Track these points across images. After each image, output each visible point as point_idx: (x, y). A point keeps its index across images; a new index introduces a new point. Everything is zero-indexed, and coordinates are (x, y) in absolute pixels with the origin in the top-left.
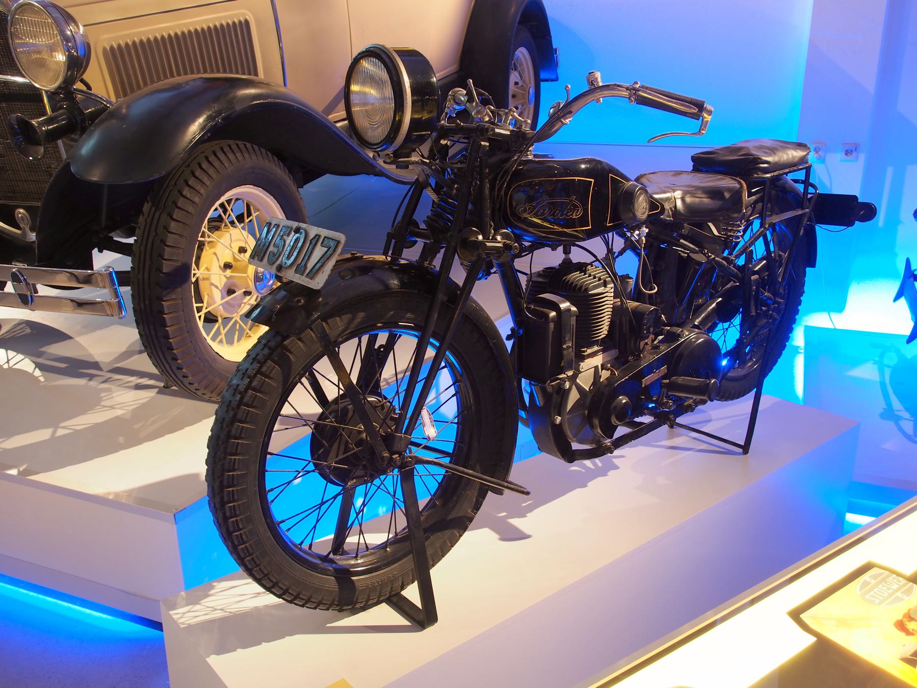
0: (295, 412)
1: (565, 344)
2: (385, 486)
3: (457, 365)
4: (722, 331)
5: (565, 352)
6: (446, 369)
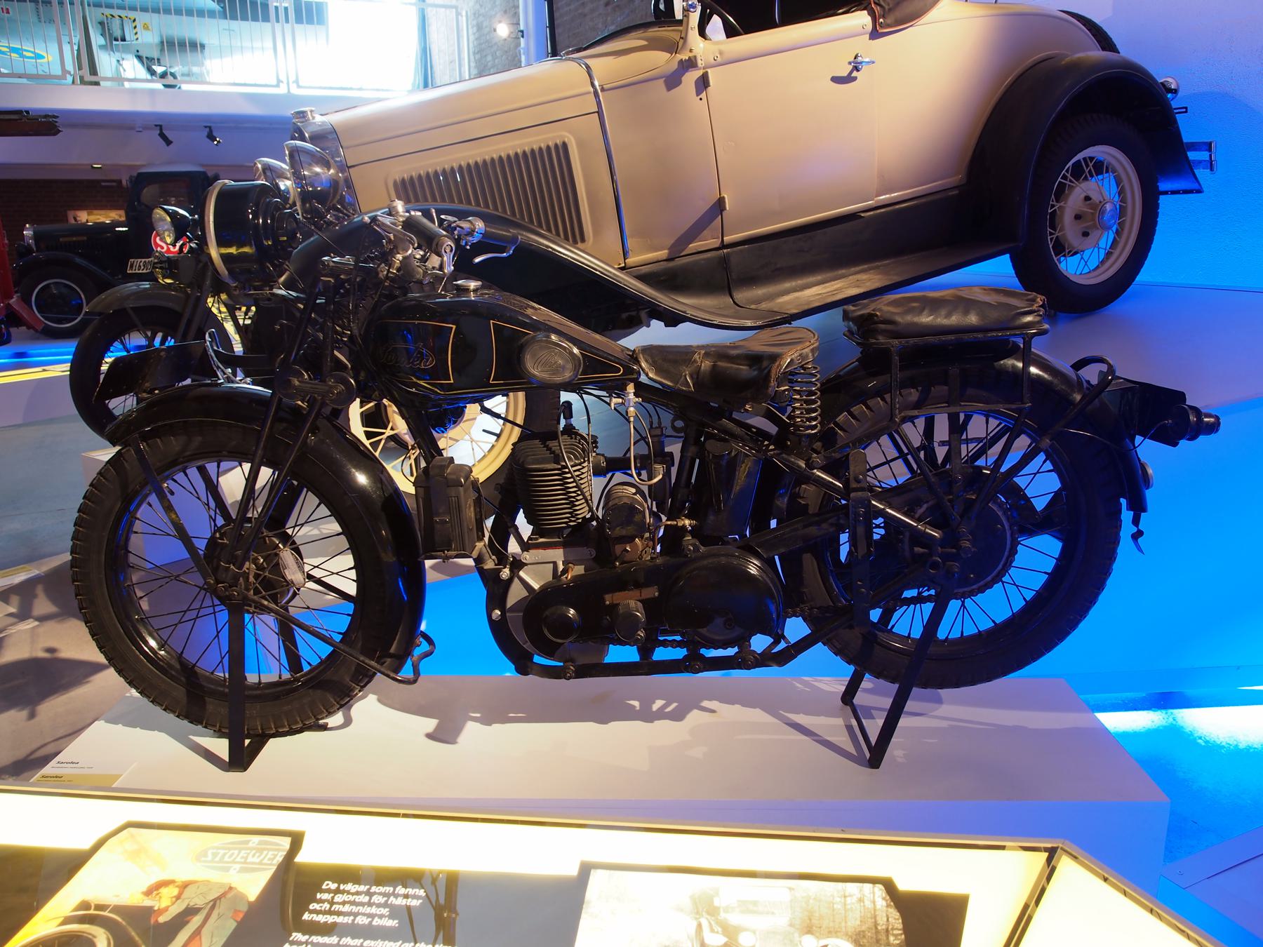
1: (438, 515)
5: (438, 526)
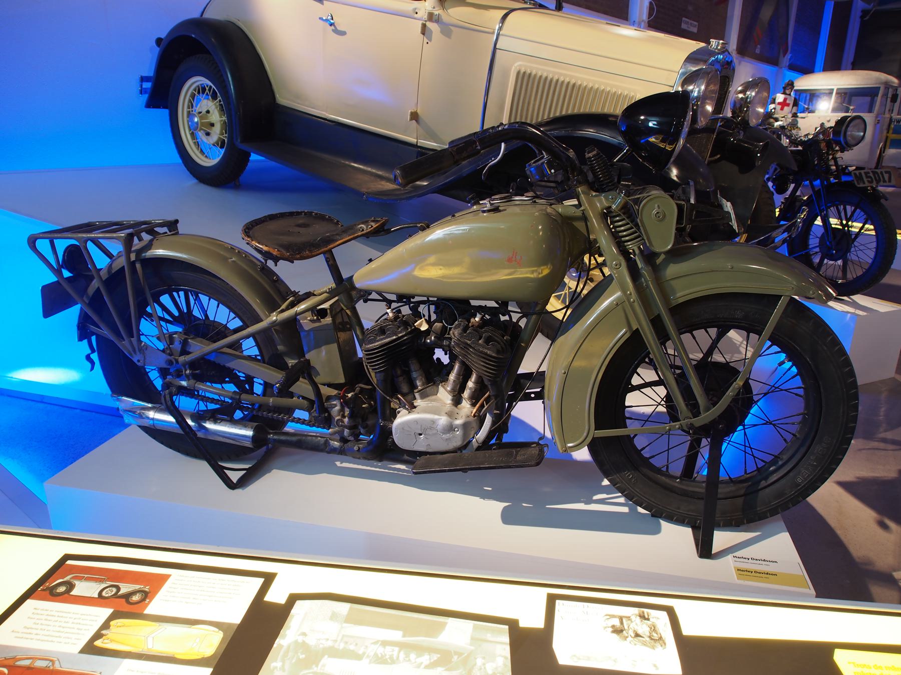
0: (543, 433)
2: (719, 350)
3: (828, 288)
4: (729, 445)
6: (268, 261)
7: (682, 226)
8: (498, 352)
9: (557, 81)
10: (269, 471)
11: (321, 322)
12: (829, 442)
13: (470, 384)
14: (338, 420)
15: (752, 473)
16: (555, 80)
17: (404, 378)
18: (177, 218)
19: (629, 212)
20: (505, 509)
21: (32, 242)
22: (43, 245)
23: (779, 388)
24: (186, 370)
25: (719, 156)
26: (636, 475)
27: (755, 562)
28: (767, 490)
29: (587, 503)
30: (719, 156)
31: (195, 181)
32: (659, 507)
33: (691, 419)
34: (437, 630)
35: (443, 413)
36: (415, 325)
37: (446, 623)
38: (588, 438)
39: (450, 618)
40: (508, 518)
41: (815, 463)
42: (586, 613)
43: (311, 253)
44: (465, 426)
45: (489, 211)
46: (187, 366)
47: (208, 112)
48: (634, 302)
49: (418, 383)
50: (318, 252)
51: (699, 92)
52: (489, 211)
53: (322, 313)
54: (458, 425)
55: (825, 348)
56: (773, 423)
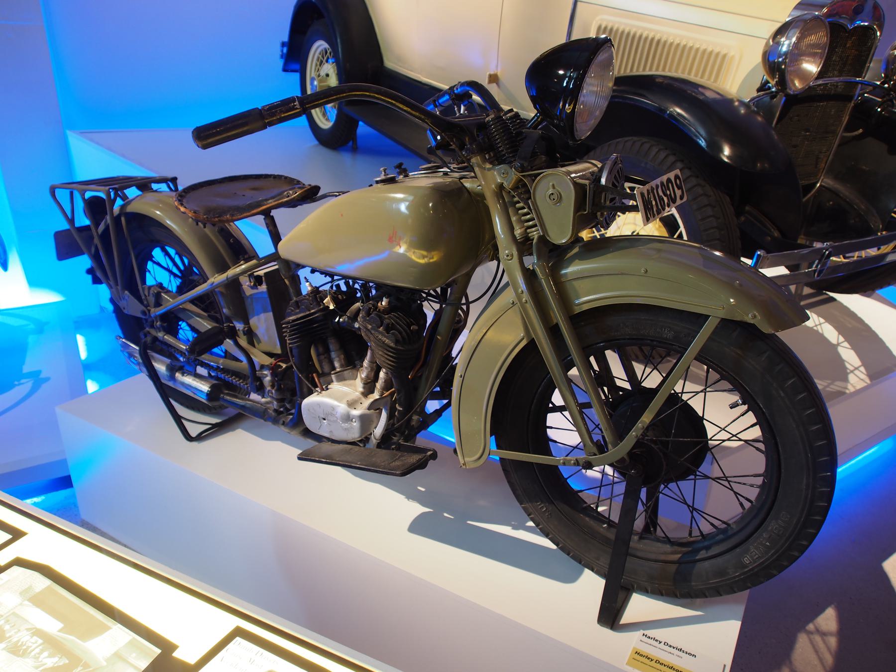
7: (586, 213)
8: (397, 342)
9: (640, 37)
10: (234, 430)
11: (257, 289)
12: (786, 519)
13: (382, 375)
14: (269, 391)
15: (697, 538)
16: (638, 35)
17: (325, 358)
18: (176, 176)
19: (524, 190)
20: (423, 515)
21: (52, 191)
22: (63, 195)
23: (737, 436)
24: (157, 322)
25: (861, 131)
26: (550, 508)
27: (667, 648)
28: (707, 564)
29: (515, 528)
30: (861, 131)
31: (316, 142)
32: (576, 552)
33: (595, 455)
34: (92, 631)
35: (345, 401)
36: (324, 302)
37: (109, 628)
38: (484, 456)
39: (119, 625)
40: (419, 527)
41: (768, 544)
42: (252, 661)
43: (232, 217)
44: (363, 419)
45: (382, 181)
46: (158, 318)
47: (327, 75)
48: (526, 302)
49: (337, 364)
50: (239, 217)
51: (789, 45)
52: (382, 181)
53: (258, 280)
54: (354, 416)
55: (782, 394)
56: (729, 479)
